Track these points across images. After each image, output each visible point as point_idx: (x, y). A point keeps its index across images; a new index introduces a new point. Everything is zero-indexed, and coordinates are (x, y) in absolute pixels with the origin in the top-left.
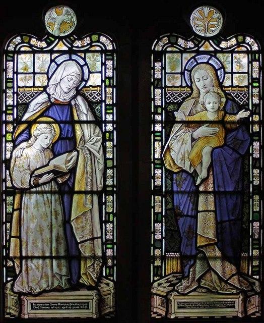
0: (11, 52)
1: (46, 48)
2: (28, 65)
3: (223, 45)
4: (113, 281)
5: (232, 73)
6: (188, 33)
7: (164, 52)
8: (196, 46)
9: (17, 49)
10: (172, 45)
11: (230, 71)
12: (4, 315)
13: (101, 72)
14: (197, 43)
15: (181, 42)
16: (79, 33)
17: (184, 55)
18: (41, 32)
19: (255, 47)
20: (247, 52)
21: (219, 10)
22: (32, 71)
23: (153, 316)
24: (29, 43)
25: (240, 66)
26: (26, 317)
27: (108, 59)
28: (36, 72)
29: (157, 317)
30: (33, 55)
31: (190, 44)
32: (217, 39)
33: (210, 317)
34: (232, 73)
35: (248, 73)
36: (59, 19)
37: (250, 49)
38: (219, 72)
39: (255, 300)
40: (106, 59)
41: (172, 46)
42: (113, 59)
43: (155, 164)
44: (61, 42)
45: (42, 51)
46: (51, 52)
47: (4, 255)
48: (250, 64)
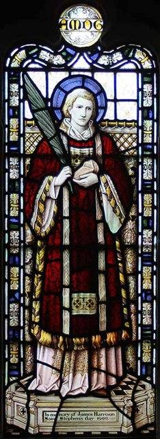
1: (29, 64)
3: (104, 60)
4: (151, 382)
5: (115, 100)
6: (57, 43)
10: (127, 58)
13: (137, 101)
15: (45, 55)
16: (106, 43)
17: (52, 75)
19: (147, 65)
20: (137, 71)
22: (113, 98)
25: (125, 89)
26: (43, 418)
32: (92, 51)
33: (84, 432)
34: (115, 100)
35: (137, 101)
36: (82, 26)
37: (140, 67)
38: (98, 97)
40: (143, 83)
41: (33, 62)
42: (151, 83)
43: (19, 223)
44: (82, 57)
46: (69, 69)
47: (6, 339)
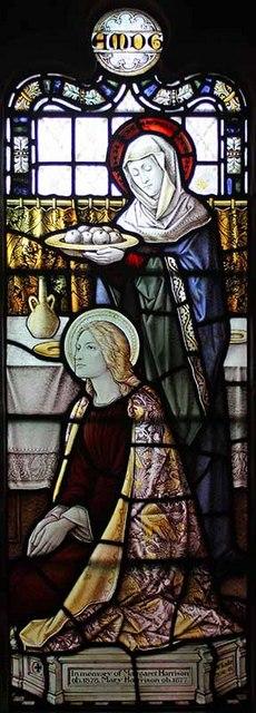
0: (22, 113)
1: (45, 104)
2: (66, 149)
7: (35, 115)
8: (109, 99)
9: (36, 108)
11: (70, 160)
12: (200, 708)
14: (109, 92)
15: (70, 90)
16: (165, 71)
18: (90, 72)
21: (118, 8)
23: (17, 699)
24: (211, 94)
27: (18, 134)
28: (70, 168)
29: (26, 703)
30: (70, 120)
31: (93, 97)
36: (129, 40)
39: (15, 672)
45: (89, 111)
48: (222, 143)
